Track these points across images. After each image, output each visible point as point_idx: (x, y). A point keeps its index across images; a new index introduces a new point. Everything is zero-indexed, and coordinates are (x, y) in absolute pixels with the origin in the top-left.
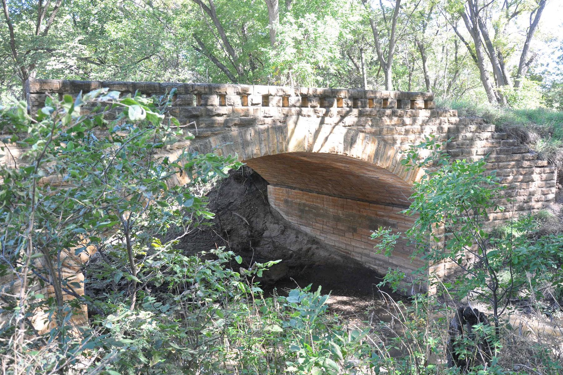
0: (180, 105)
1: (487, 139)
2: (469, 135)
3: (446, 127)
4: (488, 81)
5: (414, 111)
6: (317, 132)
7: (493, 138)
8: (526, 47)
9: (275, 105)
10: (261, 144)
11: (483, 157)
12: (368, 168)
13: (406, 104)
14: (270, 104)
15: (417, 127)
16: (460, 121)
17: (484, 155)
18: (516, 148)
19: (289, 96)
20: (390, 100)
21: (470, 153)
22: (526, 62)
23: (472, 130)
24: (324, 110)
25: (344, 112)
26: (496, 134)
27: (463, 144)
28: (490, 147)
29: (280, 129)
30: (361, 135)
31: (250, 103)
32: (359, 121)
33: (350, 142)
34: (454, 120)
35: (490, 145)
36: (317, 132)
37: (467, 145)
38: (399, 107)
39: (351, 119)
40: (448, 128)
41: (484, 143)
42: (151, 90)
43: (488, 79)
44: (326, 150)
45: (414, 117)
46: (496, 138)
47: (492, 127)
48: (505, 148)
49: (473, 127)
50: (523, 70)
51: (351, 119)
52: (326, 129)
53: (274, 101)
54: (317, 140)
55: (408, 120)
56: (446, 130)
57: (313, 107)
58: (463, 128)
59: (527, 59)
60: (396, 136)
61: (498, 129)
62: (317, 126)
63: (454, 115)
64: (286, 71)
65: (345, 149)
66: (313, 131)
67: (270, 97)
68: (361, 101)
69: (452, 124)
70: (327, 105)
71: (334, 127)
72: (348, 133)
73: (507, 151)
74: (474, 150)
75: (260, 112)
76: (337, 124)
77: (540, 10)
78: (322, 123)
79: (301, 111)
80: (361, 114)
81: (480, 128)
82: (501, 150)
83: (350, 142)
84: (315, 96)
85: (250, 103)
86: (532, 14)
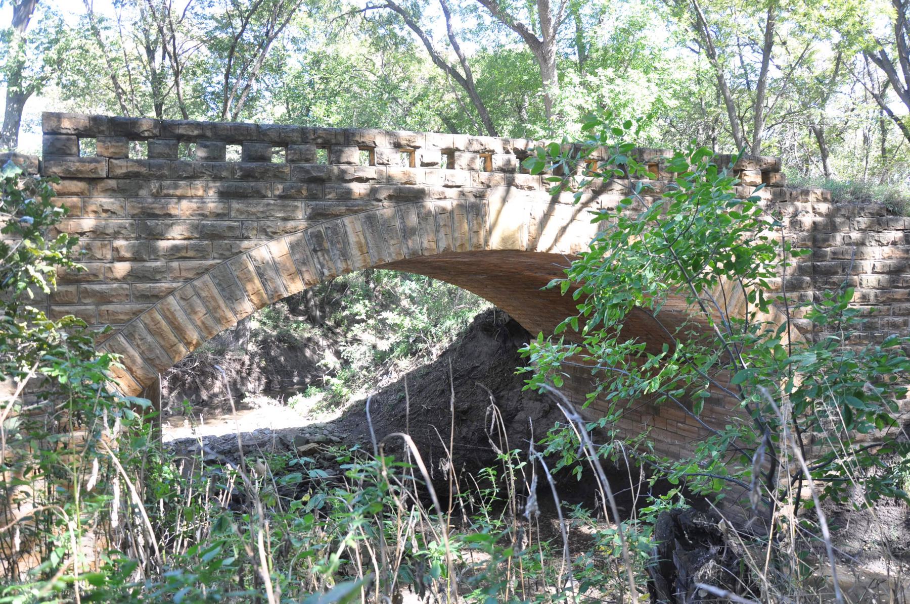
6: (547, 216)
14: (456, 166)
23: (863, 226)
36: (547, 216)
54: (545, 231)
62: (545, 207)
69: (820, 214)
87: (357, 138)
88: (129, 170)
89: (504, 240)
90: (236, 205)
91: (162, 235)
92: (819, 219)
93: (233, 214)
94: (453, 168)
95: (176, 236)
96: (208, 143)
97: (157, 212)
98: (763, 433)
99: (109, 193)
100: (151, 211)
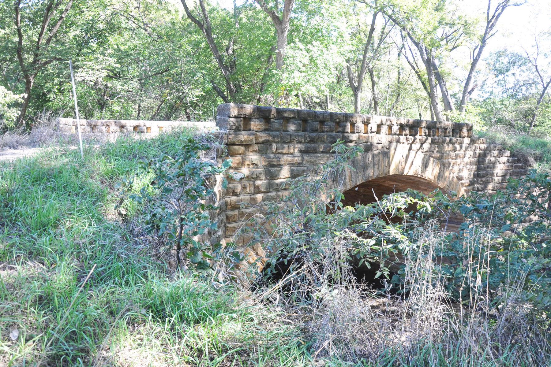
0: (327, 132)
1: (504, 163)
2: (493, 159)
3: (478, 151)
4: (437, 106)
5: (461, 139)
6: (407, 157)
7: (508, 162)
8: (469, 78)
9: (384, 133)
10: (374, 167)
11: (501, 178)
12: (423, 187)
13: (457, 133)
14: (381, 133)
15: (462, 152)
16: (487, 147)
17: (502, 176)
18: (523, 170)
19: (393, 125)
20: (448, 130)
21: (492, 174)
22: (469, 90)
23: (495, 155)
24: (412, 138)
25: (424, 139)
26: (510, 159)
27: (488, 167)
28: (506, 170)
29: (386, 154)
30: (432, 159)
31: (369, 131)
32: (430, 148)
33: (425, 165)
34: (483, 146)
35: (506, 168)
36: (407, 157)
37: (491, 168)
38: (453, 136)
39: (426, 146)
40: (479, 154)
41: (502, 166)
42: (310, 117)
43: (437, 104)
44: (411, 173)
45: (461, 143)
46: (510, 163)
47: (508, 153)
48: (516, 171)
49: (496, 153)
50: (466, 98)
51: (426, 146)
52: (413, 153)
53: (384, 129)
54: (407, 164)
55: (458, 147)
56: (478, 155)
57: (406, 135)
58: (488, 153)
59: (470, 88)
60: (450, 160)
61: (512, 155)
62: (407, 152)
63: (484, 143)
64: (294, 93)
65: (422, 172)
66: (405, 157)
67: (382, 126)
68: (433, 131)
69: (481, 150)
70: (413, 133)
71: (416, 153)
72: (424, 158)
73: (518, 173)
74: (495, 172)
75: (374, 139)
76: (418, 150)
77: (481, 48)
78: (410, 149)
79: (399, 139)
80: (433, 142)
81: (501, 152)
82: (513, 172)
83: (425, 165)
84: (407, 126)
85: (369, 131)
86: (474, 50)
87: (351, 119)
88: (265, 139)
89: (397, 168)
90: (306, 158)
91: (276, 176)
92: (481, 152)
93: (304, 163)
94: (380, 134)
95: (285, 173)
96: (296, 122)
97: (275, 163)
98: (196, 75)
99: (255, 153)
100: (272, 163)
